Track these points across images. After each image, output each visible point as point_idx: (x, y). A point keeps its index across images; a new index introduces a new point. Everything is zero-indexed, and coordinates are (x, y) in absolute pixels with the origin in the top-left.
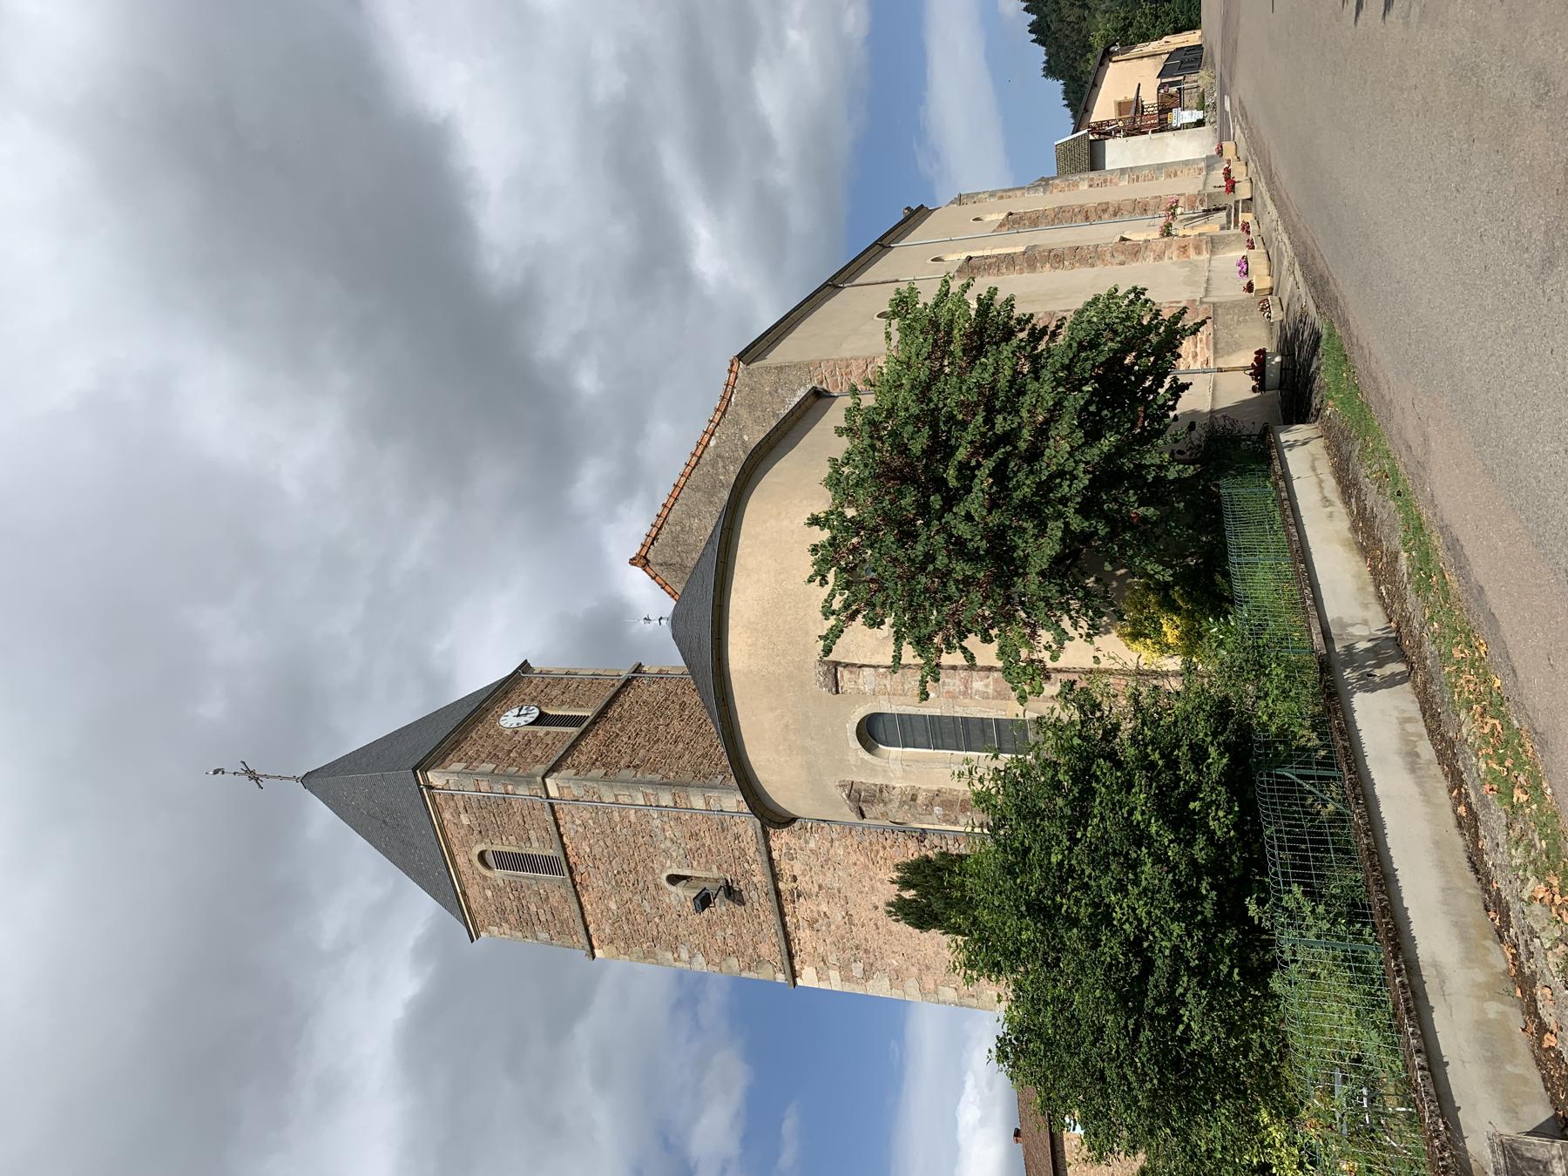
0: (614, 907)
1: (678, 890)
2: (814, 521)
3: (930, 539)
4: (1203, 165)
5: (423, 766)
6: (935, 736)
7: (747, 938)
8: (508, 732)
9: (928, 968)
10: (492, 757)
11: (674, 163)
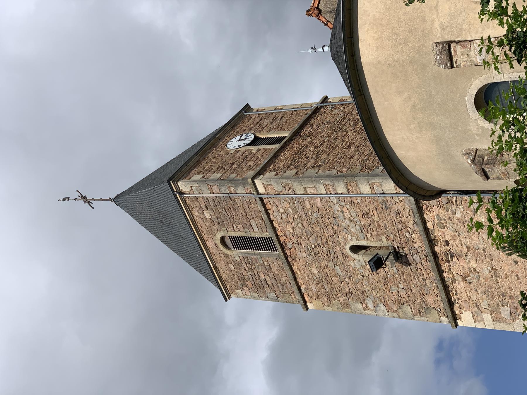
0: (315, 272)
5: (175, 178)
8: (232, 152)
10: (221, 169)
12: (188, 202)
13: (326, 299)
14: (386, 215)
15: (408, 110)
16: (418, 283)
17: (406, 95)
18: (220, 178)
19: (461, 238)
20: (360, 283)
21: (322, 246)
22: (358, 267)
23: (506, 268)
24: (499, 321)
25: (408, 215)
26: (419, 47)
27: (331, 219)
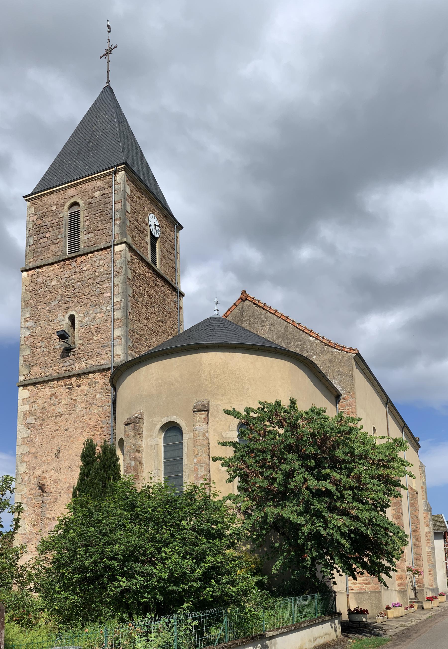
0: (53, 283)
1: (66, 322)
2: (293, 402)
3: (293, 461)
4: (434, 587)
5: (128, 169)
6: (171, 461)
7: (42, 360)
8: (146, 220)
9: (36, 457)
10: (134, 210)
11: (432, 303)
12: (108, 177)
13: (31, 288)
14: (98, 346)
15: (170, 380)
16: (48, 363)
17: (180, 380)
18: (127, 212)
19: (82, 396)
20: (46, 318)
21: (74, 292)
22: (58, 319)
23: (62, 423)
24: (24, 415)
25: (98, 361)
26: (208, 391)
27: (95, 303)
